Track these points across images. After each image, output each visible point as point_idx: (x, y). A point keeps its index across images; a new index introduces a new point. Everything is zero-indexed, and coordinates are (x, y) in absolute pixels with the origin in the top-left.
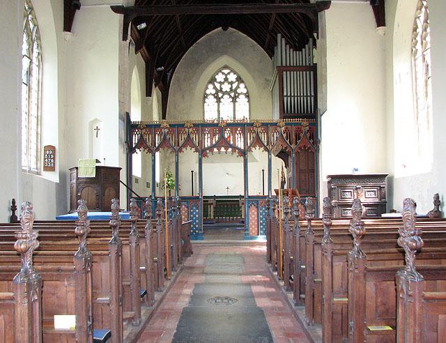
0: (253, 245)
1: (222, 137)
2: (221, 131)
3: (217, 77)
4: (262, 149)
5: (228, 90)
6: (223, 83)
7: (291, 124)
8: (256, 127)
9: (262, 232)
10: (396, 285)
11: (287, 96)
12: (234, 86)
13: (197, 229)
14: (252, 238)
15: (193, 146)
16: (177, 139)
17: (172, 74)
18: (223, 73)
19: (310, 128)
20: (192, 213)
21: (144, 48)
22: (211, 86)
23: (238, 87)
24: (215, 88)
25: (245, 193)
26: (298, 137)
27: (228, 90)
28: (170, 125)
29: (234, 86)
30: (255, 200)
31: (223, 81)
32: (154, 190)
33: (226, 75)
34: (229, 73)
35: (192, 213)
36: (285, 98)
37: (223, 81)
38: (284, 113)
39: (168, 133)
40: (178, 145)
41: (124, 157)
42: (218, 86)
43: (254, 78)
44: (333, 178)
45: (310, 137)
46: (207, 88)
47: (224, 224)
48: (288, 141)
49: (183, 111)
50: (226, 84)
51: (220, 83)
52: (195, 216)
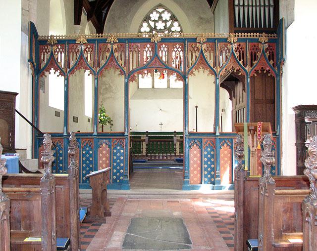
0: (195, 197)
1: (155, 56)
2: (155, 48)
3: (151, 15)
4: (207, 72)
5: (163, 28)
6: (158, 21)
7: (245, 40)
8: (200, 43)
9: (206, 179)
10: (301, 210)
11: (239, 5)
12: (169, 24)
13: (121, 175)
14: (193, 188)
15: (118, 67)
16: (96, 58)
17: (107, 11)
18: (158, 12)
19: (269, 46)
20: (115, 154)
21: (94, 16)
22: (145, 24)
23: (172, 25)
24: (149, 26)
25: (185, 129)
26: (254, 57)
27: (163, 28)
28: (87, 40)
29: (169, 24)
30: (198, 137)
31: (157, 19)
32: (66, 123)
33: (160, 14)
34: (163, 12)
35: (115, 154)
36: (237, 9)
37: (157, 19)
38: (235, 27)
39: (85, 50)
40: (99, 65)
41: (29, 81)
42: (152, 24)
43: (188, 15)
44: (302, 111)
45: (269, 56)
46: (141, 26)
47: (157, 163)
48: (241, 62)
49: (111, 34)
50: (160, 22)
51: (155, 21)
52: (118, 158)
